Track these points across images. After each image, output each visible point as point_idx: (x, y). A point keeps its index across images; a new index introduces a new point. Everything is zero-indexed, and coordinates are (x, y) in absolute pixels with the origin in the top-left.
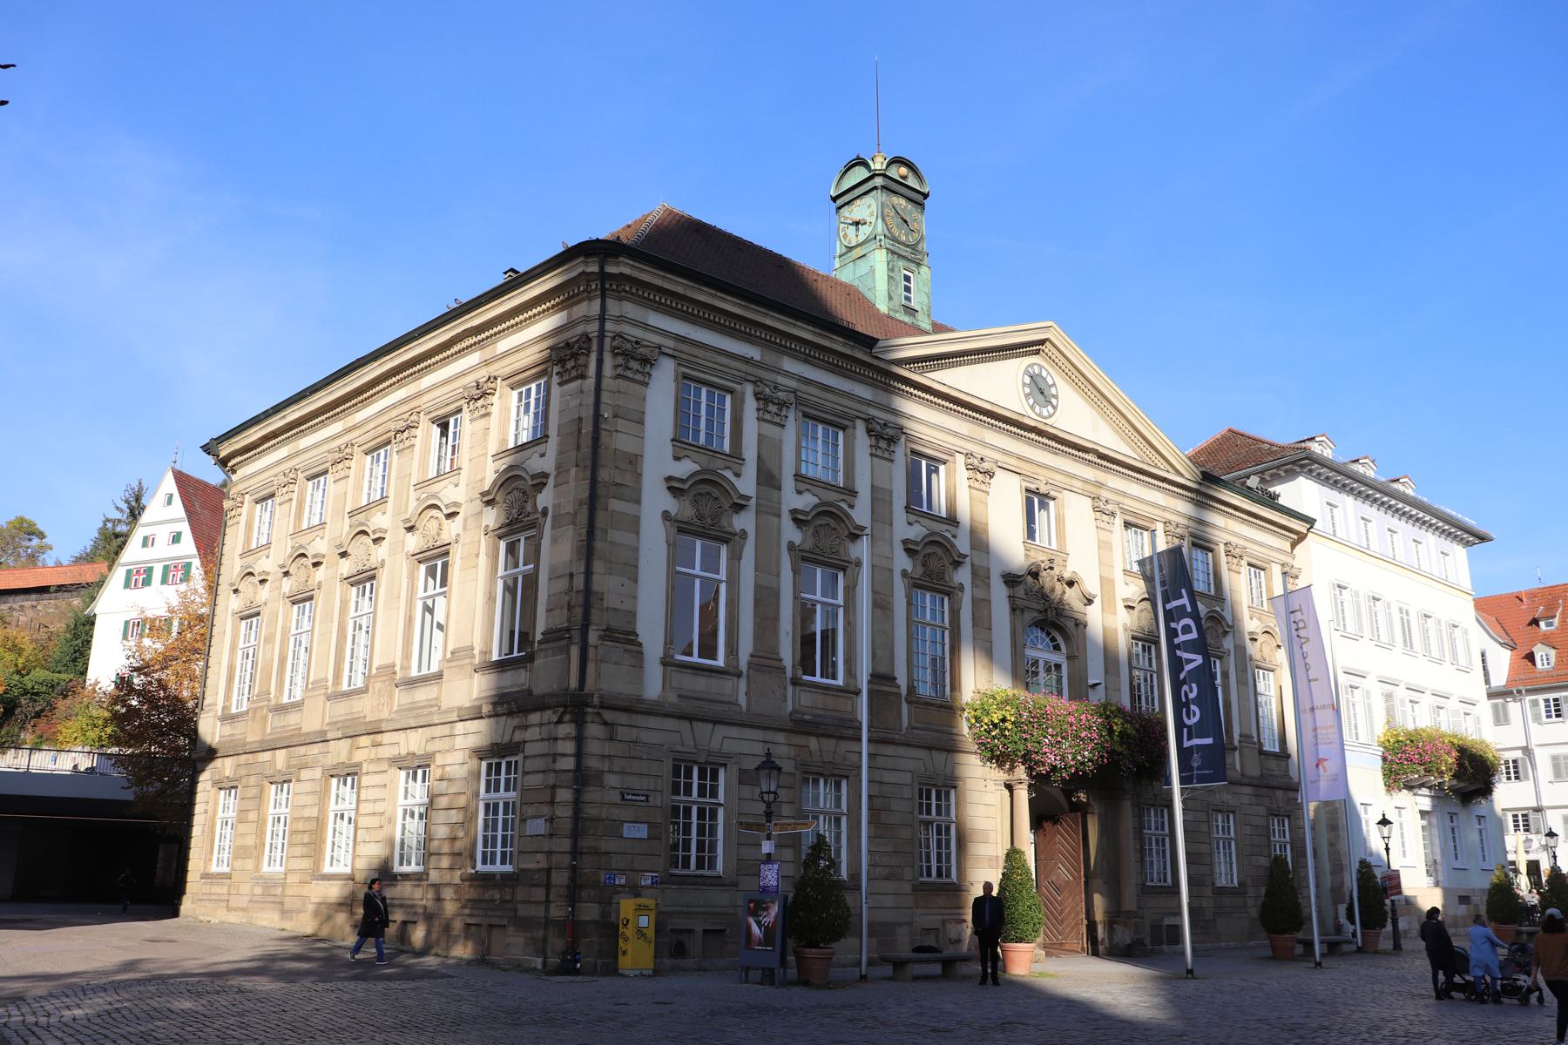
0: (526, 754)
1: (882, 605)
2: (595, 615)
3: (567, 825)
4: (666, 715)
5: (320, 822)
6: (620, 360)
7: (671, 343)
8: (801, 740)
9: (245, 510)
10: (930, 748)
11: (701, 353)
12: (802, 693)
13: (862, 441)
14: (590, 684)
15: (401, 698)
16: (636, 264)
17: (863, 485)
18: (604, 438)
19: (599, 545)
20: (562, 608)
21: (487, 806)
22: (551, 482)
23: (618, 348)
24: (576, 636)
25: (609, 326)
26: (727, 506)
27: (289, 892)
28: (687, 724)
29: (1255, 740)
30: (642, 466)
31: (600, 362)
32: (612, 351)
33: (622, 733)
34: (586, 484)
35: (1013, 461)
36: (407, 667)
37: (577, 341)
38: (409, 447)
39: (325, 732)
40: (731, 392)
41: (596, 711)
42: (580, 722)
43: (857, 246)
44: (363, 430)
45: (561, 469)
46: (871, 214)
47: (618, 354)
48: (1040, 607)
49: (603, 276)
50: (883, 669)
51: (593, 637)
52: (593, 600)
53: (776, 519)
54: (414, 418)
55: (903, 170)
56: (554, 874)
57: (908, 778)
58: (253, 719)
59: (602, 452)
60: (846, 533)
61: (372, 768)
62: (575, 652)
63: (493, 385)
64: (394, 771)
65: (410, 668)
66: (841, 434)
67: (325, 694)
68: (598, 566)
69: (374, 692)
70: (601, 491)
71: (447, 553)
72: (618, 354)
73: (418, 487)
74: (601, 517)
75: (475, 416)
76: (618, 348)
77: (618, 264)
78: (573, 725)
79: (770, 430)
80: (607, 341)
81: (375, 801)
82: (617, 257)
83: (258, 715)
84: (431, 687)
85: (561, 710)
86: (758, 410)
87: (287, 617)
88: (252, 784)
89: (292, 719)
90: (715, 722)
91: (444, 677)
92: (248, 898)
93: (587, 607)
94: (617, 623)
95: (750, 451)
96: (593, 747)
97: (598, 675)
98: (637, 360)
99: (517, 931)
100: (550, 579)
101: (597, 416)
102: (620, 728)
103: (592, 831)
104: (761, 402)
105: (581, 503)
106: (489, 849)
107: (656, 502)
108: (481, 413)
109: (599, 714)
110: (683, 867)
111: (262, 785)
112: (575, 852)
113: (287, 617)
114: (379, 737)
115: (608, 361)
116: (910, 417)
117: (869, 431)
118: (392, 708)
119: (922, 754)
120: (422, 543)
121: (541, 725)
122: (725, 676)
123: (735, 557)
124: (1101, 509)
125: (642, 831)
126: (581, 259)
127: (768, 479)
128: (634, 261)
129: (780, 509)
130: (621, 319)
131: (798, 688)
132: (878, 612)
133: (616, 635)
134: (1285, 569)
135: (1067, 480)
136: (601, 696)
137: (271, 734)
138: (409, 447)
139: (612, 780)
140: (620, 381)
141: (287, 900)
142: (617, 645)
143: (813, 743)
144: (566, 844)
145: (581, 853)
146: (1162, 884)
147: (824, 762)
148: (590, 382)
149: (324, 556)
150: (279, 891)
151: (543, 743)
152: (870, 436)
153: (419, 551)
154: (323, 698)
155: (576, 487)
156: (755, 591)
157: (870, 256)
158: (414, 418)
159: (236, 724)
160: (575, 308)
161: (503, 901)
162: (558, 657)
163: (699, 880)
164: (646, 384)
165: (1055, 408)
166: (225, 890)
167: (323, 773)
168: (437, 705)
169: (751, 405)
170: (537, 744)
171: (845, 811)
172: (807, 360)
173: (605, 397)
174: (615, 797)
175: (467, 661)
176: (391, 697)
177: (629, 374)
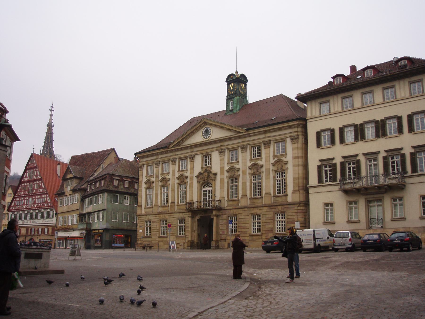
1: (173, 190)
7: (145, 162)
8: (160, 215)
11: (148, 162)
21: (146, 228)
30: (414, 112)
35: (199, 152)
71: (260, 174)
106: (283, 229)
107: (144, 186)
116: (337, 103)
125: (141, 231)
135: (212, 149)
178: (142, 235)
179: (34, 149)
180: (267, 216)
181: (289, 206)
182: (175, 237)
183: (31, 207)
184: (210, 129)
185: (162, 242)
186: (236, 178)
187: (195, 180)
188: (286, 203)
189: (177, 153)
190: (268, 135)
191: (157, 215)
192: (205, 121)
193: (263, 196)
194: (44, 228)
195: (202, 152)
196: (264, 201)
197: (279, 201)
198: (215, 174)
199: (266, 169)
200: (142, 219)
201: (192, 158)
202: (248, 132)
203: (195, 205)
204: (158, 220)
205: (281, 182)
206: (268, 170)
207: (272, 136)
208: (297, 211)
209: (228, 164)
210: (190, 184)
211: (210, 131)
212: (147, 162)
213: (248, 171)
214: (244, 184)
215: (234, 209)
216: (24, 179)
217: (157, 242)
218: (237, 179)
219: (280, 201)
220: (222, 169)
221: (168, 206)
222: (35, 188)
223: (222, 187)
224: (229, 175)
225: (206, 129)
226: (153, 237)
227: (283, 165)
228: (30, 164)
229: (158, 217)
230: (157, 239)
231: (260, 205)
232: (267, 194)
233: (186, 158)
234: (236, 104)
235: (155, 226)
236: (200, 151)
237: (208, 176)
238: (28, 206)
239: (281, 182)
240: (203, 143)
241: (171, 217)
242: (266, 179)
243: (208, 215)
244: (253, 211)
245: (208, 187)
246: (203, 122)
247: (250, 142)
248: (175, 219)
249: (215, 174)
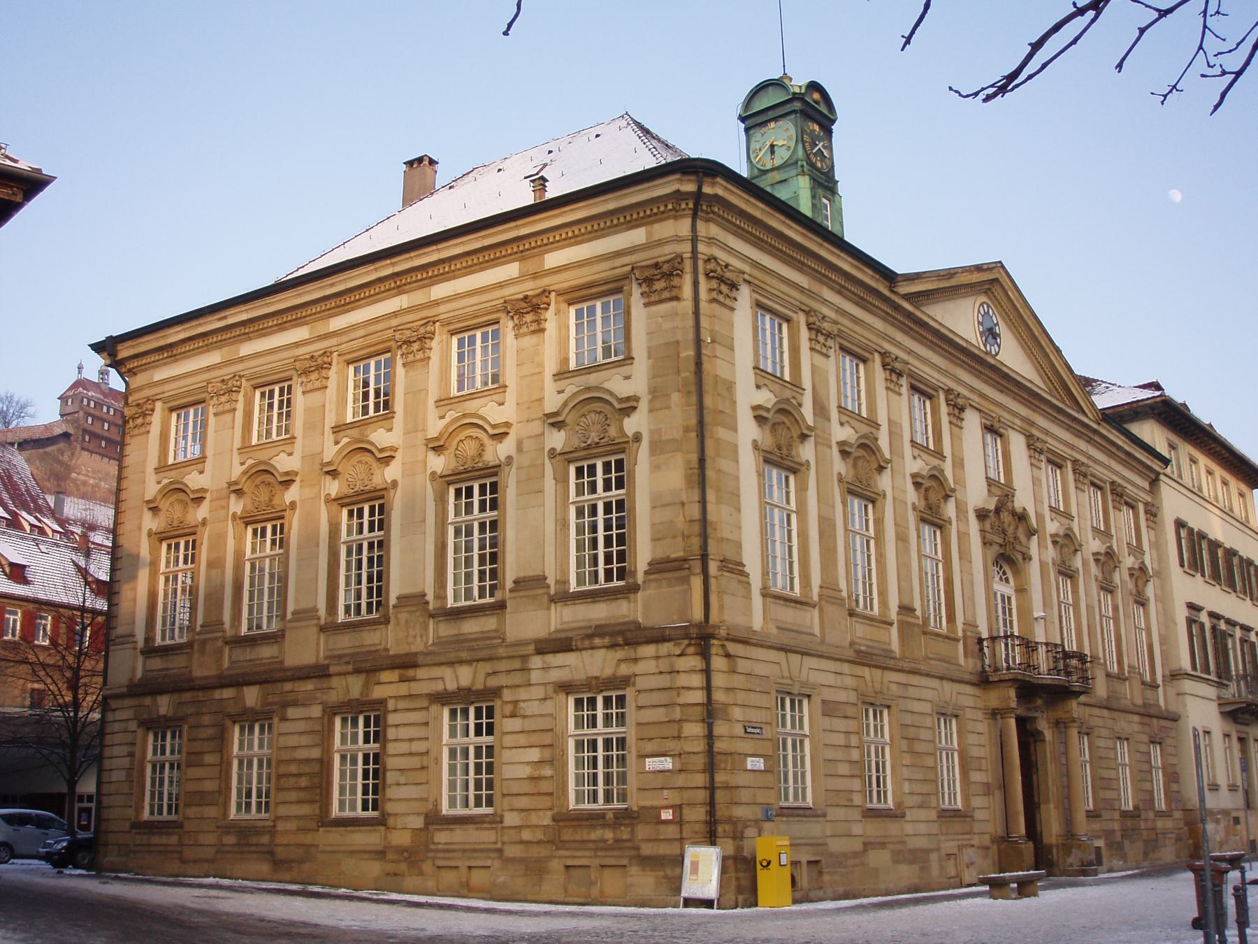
0: (638, 688)
2: (712, 548)
3: (700, 761)
4: (770, 647)
5: (324, 765)
6: (714, 284)
9: (156, 419)
10: (941, 678)
11: (768, 279)
12: (857, 625)
13: (880, 374)
14: (714, 617)
15: (446, 630)
16: (729, 186)
17: (882, 419)
18: (706, 366)
19: (710, 473)
20: (674, 537)
22: (643, 406)
23: (712, 271)
24: (697, 567)
25: (701, 248)
26: (795, 435)
27: (283, 840)
28: (782, 654)
29: (1102, 661)
31: (696, 284)
32: (707, 275)
33: (742, 665)
34: (693, 410)
36: (441, 596)
37: (668, 261)
38: (422, 360)
39: (327, 666)
40: (788, 320)
41: (720, 643)
42: (705, 654)
43: (772, 170)
44: (345, 338)
45: (657, 394)
46: (789, 138)
47: (713, 277)
48: (1000, 541)
49: (698, 196)
50: (906, 602)
51: (713, 567)
52: (709, 530)
53: (829, 450)
54: (430, 328)
55: (816, 96)
56: (686, 811)
58: (202, 651)
59: (704, 377)
60: (876, 466)
61: (401, 705)
62: (697, 583)
63: (545, 299)
64: (434, 708)
65: (445, 597)
66: (861, 366)
67: (317, 625)
68: (711, 496)
69: (398, 624)
70: (708, 418)
72: (713, 277)
73: (442, 403)
74: (709, 444)
75: (521, 331)
76: (712, 271)
77: (713, 184)
78: (698, 658)
79: (819, 360)
80: (700, 263)
81: (411, 740)
82: (714, 176)
83: (209, 648)
84: (488, 618)
85: (686, 642)
86: (811, 340)
87: (240, 540)
88: (206, 723)
89: (266, 652)
90: (803, 654)
91: (509, 609)
92: (213, 850)
93: (704, 536)
94: (729, 553)
95: (807, 382)
96: (718, 680)
97: (721, 607)
98: (726, 283)
99: (644, 871)
100: (654, 507)
101: (698, 342)
102: (739, 660)
103: (723, 766)
104: (814, 332)
105: (687, 430)
107: (748, 432)
108: (532, 328)
109: (723, 646)
111: (223, 726)
112: (711, 788)
113: (240, 540)
114: (411, 673)
115: (703, 285)
117: (884, 366)
118: (427, 640)
120: (455, 464)
121: (657, 658)
122: (806, 608)
123: (802, 488)
124: (1033, 445)
125: (759, 764)
126: (677, 176)
127: (820, 409)
128: (727, 182)
129: (830, 441)
130: (712, 241)
131: (854, 619)
132: (900, 543)
133: (730, 566)
136: (728, 628)
137: (228, 669)
138: (422, 360)
139: (737, 713)
140: (715, 305)
141: (279, 849)
142: (733, 576)
143: (866, 672)
144: (700, 779)
145: (705, 788)
146: (586, 806)
147: (876, 692)
148: (687, 305)
149: (296, 474)
150: (265, 839)
151: (662, 676)
152: (885, 369)
153: (450, 472)
154: (315, 630)
155: (679, 413)
156: (819, 523)
157: (792, 182)
158: (430, 328)
159: (171, 657)
160: (657, 227)
161: (617, 841)
162: (677, 588)
163: (801, 812)
164: (732, 309)
165: (999, 346)
166: (174, 840)
167: (324, 711)
168: (500, 638)
169: (804, 334)
170: (652, 677)
171: (888, 740)
173: (704, 323)
174: (739, 730)
175: (541, 591)
176: (426, 628)
177: (721, 298)
178: (762, 797)
182: (933, 815)
185: (882, 845)
186: (376, 504)
187: (974, 526)
191: (846, 668)
200: (760, 669)
204: (852, 697)
208: (680, 731)
209: (158, 470)
217: (857, 845)
218: (382, 507)
229: (849, 681)
230: (857, 829)
235: (839, 739)
241: (912, 692)
248: (927, 708)
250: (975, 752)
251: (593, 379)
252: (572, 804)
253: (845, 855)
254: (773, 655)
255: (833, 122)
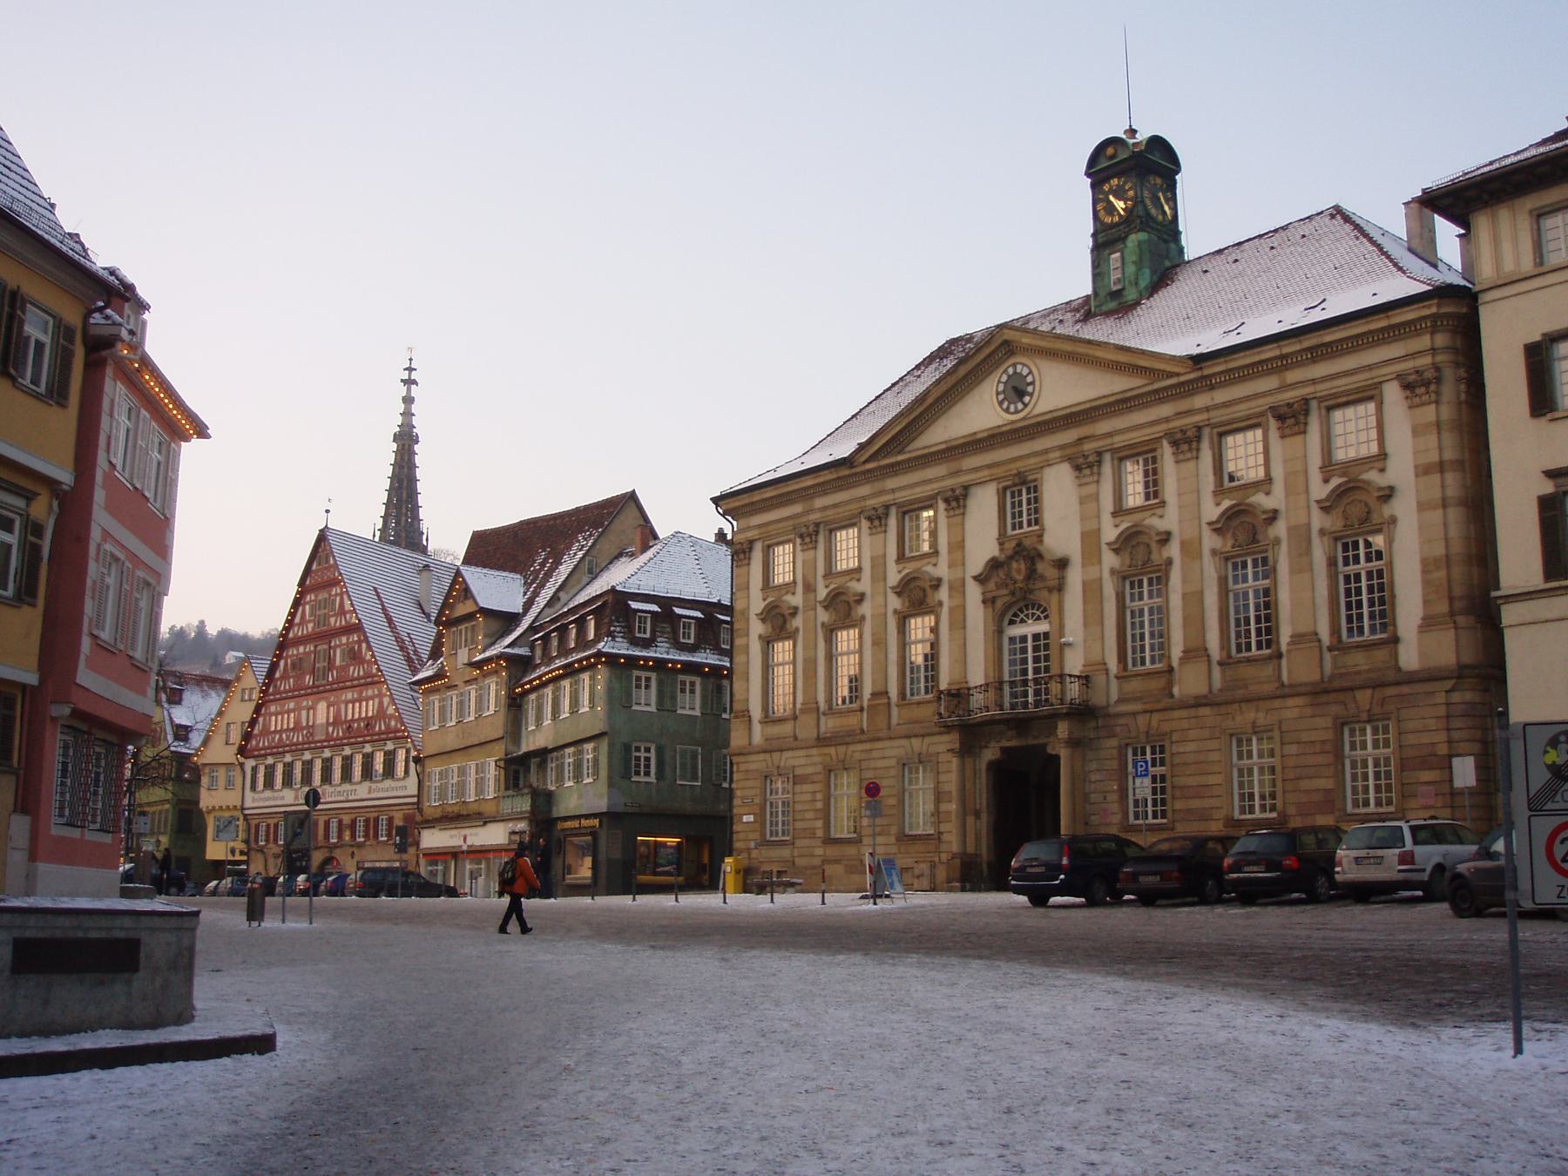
8: (826, 750)
57: (893, 762)
110: (1237, 563)
119: (904, 742)
125: (751, 818)
134: (1005, 1104)
143: (832, 750)
172: (825, 493)
179: (327, 511)
180: (1305, 737)
181: (1405, 689)
183: (323, 738)
184: (1030, 372)
187: (974, 593)
188: (1391, 675)
189: (891, 483)
190: (1293, 376)
192: (1005, 337)
193: (1284, 648)
194: (375, 815)
195: (999, 471)
196: (1290, 672)
197: (1358, 668)
198: (1062, 564)
199: (1290, 529)
200: (753, 766)
201: (957, 500)
202: (1201, 369)
203: (977, 700)
205: (1364, 584)
206: (1301, 535)
207: (1314, 381)
210: (951, 610)
211: (1029, 379)
212: (824, 514)
213: (1210, 541)
214: (1194, 600)
215: (1152, 712)
216: (296, 629)
219: (1366, 667)
220: (1090, 539)
221: (1280, 656)
222: (338, 662)
223: (1093, 618)
224: (1122, 564)
225: (1011, 371)
226: (798, 843)
227: (1372, 502)
228: (317, 571)
230: (819, 851)
231: (1268, 688)
232: (1297, 639)
233: (928, 503)
234: (1134, 263)
236: (989, 466)
237: (1032, 574)
238: (311, 735)
239: (1364, 584)
240: (1002, 433)
241: (875, 754)
242: (1292, 572)
243: (1036, 742)
244: (1238, 718)
245: (1030, 621)
246: (999, 342)
247: (1213, 414)
249: (1062, 564)
250: (946, 788)
251: (1137, 517)
252: (1349, 808)
253: (806, 868)
254: (761, 757)
255: (1177, 172)
